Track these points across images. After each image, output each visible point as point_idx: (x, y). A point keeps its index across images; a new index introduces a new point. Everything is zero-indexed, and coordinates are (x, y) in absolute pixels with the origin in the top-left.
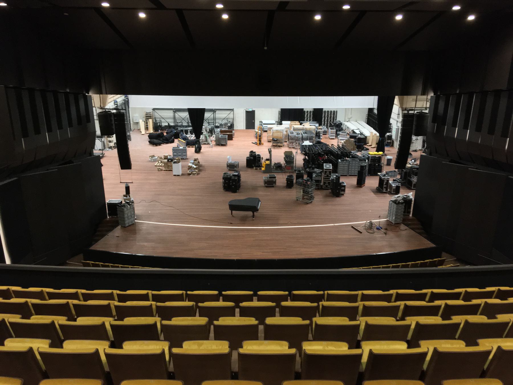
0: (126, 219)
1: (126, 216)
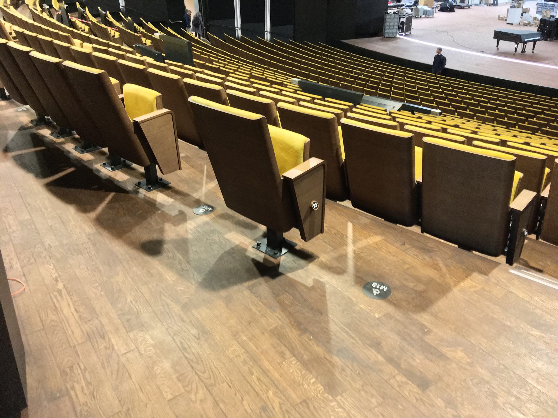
0: (387, 28)
1: (387, 24)
